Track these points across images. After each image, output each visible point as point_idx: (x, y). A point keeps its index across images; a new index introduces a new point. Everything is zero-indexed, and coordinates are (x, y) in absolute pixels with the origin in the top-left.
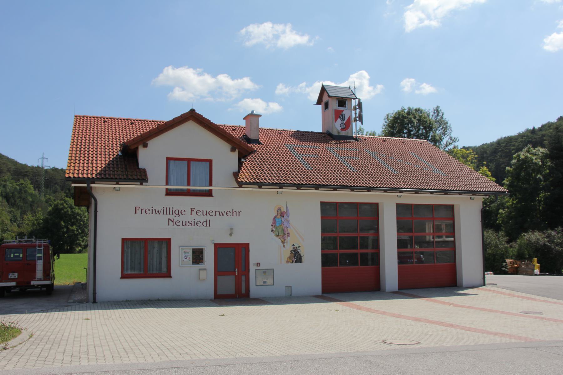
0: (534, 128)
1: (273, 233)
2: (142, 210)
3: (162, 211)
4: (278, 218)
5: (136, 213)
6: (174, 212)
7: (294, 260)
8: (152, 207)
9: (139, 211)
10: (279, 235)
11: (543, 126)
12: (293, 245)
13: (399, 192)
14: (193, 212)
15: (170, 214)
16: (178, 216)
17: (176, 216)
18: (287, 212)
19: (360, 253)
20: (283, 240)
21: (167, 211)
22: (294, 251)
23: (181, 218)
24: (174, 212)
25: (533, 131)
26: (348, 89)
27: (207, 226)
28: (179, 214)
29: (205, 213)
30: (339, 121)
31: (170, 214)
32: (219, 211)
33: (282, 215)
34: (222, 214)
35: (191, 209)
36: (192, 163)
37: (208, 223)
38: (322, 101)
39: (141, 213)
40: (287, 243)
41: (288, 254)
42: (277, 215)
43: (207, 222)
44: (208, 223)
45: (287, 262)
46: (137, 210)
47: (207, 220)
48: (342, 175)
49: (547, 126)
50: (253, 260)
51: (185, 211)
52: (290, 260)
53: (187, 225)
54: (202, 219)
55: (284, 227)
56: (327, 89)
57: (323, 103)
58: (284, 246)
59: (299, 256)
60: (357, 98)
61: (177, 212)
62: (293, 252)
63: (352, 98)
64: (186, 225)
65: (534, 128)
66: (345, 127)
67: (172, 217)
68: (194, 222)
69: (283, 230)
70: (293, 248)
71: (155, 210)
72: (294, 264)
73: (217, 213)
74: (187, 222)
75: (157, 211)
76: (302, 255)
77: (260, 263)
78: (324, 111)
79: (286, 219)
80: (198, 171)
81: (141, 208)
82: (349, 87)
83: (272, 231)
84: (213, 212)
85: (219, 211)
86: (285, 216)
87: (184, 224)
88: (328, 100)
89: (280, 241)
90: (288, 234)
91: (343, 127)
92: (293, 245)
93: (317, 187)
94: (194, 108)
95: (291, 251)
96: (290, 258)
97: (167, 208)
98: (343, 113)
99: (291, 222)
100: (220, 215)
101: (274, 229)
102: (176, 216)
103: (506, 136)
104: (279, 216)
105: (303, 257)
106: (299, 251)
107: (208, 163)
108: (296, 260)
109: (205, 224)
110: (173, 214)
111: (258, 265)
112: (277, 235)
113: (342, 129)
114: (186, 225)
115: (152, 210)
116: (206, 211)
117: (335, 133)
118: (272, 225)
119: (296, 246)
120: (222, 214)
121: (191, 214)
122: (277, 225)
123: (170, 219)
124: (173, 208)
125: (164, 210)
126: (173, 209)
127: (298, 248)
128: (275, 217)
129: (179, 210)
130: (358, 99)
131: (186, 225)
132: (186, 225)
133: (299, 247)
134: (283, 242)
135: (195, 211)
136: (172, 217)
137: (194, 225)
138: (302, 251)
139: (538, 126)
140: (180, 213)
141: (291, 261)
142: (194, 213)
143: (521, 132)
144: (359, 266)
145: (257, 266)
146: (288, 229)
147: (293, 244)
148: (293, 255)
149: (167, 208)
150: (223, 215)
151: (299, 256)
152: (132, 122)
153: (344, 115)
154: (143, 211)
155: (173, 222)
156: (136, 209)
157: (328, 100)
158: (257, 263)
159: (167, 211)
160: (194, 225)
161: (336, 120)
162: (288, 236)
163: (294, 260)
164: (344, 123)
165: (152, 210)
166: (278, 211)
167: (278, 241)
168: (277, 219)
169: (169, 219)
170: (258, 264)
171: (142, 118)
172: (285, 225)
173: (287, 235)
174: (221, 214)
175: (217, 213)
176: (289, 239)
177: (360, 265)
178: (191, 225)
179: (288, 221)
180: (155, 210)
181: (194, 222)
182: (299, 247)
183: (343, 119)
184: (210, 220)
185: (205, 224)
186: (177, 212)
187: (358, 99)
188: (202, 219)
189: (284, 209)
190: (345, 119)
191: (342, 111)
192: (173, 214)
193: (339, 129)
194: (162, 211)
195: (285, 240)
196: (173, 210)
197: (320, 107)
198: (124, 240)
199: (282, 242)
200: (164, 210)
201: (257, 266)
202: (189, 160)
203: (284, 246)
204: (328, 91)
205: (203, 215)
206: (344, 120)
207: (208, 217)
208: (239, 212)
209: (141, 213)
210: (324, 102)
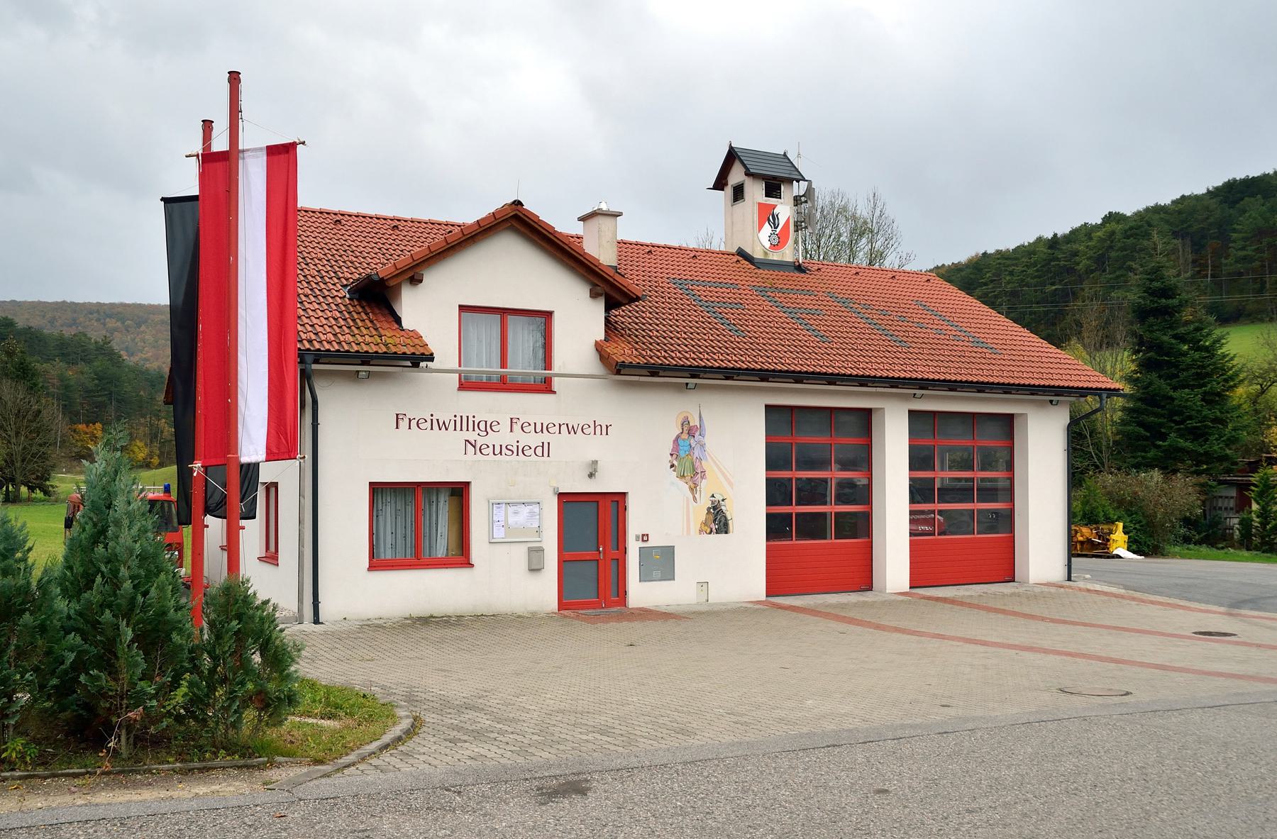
0: (1055, 235)
1: (674, 471)
2: (410, 420)
3: (453, 422)
4: (684, 440)
5: (397, 428)
6: (477, 425)
7: (714, 527)
8: (432, 415)
9: (404, 424)
10: (685, 474)
11: (1074, 232)
12: (713, 496)
13: (645, 372)
14: (514, 425)
15: (468, 430)
16: (485, 433)
17: (481, 433)
18: (700, 427)
19: (836, 513)
20: (692, 486)
21: (462, 423)
22: (714, 508)
23: (492, 439)
24: (477, 425)
25: (1054, 242)
26: (782, 157)
27: (543, 456)
28: (486, 430)
29: (538, 429)
30: (767, 229)
31: (468, 430)
32: (567, 425)
33: (691, 433)
34: (445, 426)
35: (511, 419)
36: (511, 319)
37: (545, 449)
38: (726, 184)
39: (410, 428)
40: (700, 491)
41: (702, 515)
42: (682, 433)
43: (543, 447)
44: (545, 449)
45: (701, 531)
46: (400, 421)
47: (543, 443)
48: (632, 338)
49: (1084, 231)
50: (634, 527)
51: (499, 424)
52: (706, 527)
53: (503, 453)
54: (533, 440)
55: (695, 458)
56: (739, 154)
57: (729, 190)
58: (695, 499)
59: (723, 520)
60: (804, 180)
61: (482, 426)
62: (712, 510)
63: (793, 180)
64: (501, 453)
65: (1055, 235)
66: (779, 242)
67: (472, 436)
68: (518, 446)
69: (693, 466)
70: (713, 503)
71: (438, 420)
72: (714, 536)
73: (564, 428)
74: (504, 450)
75: (441, 424)
76: (729, 518)
77: (647, 535)
78: (732, 206)
79: (698, 442)
80: (523, 339)
81: (408, 416)
82: (785, 153)
83: (672, 466)
84: (555, 426)
85: (567, 425)
86: (697, 434)
87: (497, 451)
88: (744, 180)
89: (687, 486)
90: (703, 474)
91: (775, 242)
92: (713, 496)
93: (764, 375)
94: (519, 199)
95: (709, 509)
96: (705, 524)
97: (461, 417)
98: (776, 211)
99: (707, 447)
100: (569, 433)
101: (675, 463)
102: (481, 433)
103: (991, 251)
104: (685, 436)
105: (730, 522)
106: (723, 508)
107: (541, 320)
108: (717, 527)
109: (539, 451)
110: (474, 430)
111: (645, 538)
112: (682, 474)
113: (773, 246)
114: (501, 455)
115: (432, 420)
116: (542, 424)
117: (758, 254)
118: (672, 455)
119: (718, 497)
120: (445, 426)
121: (511, 431)
122: (682, 454)
123: (468, 441)
124: (474, 417)
125: (455, 421)
126: (474, 419)
127: (721, 502)
128: (678, 437)
129: (486, 422)
130: (807, 181)
131: (501, 453)
132: (501, 455)
133: (723, 500)
134: (693, 490)
135: (519, 424)
136: (472, 436)
137: (518, 455)
138: (729, 510)
139: (1063, 229)
140: (489, 427)
141: (709, 531)
142: (517, 428)
143: (1026, 244)
144: (832, 541)
145: (643, 540)
146: (703, 462)
147: (711, 494)
148: (712, 518)
149: (461, 417)
150: (447, 429)
151: (723, 520)
152: (396, 224)
153: (777, 216)
154: (414, 423)
155: (474, 447)
156: (397, 419)
157: (744, 180)
158: (643, 535)
159: (462, 423)
160: (518, 455)
161: (760, 227)
162: (702, 478)
163: (714, 527)
164: (777, 233)
165: (432, 420)
166: (682, 425)
167: (684, 487)
168: (680, 442)
169: (466, 440)
170: (645, 537)
171: (354, 211)
172: (697, 453)
173: (699, 475)
174: (572, 430)
175: (564, 428)
176: (703, 484)
177: (835, 539)
178: (511, 453)
179: (703, 446)
180: (438, 420)
181: (518, 446)
182: (723, 500)
183: (774, 224)
184: (549, 443)
185: (539, 451)
186: (482, 426)
187: (807, 181)
188: (533, 440)
189: (695, 422)
190: (778, 225)
191: (774, 207)
192: (474, 430)
193: (767, 245)
194: (452, 423)
195: (696, 485)
196: (474, 421)
197: (723, 196)
198: (376, 489)
199: (691, 489)
200: (455, 421)
201: (643, 540)
202: (504, 312)
203: (695, 499)
204: (742, 158)
205: (536, 432)
206: (776, 228)
207: (545, 437)
208: (607, 427)
209: (410, 428)
210: (732, 186)
